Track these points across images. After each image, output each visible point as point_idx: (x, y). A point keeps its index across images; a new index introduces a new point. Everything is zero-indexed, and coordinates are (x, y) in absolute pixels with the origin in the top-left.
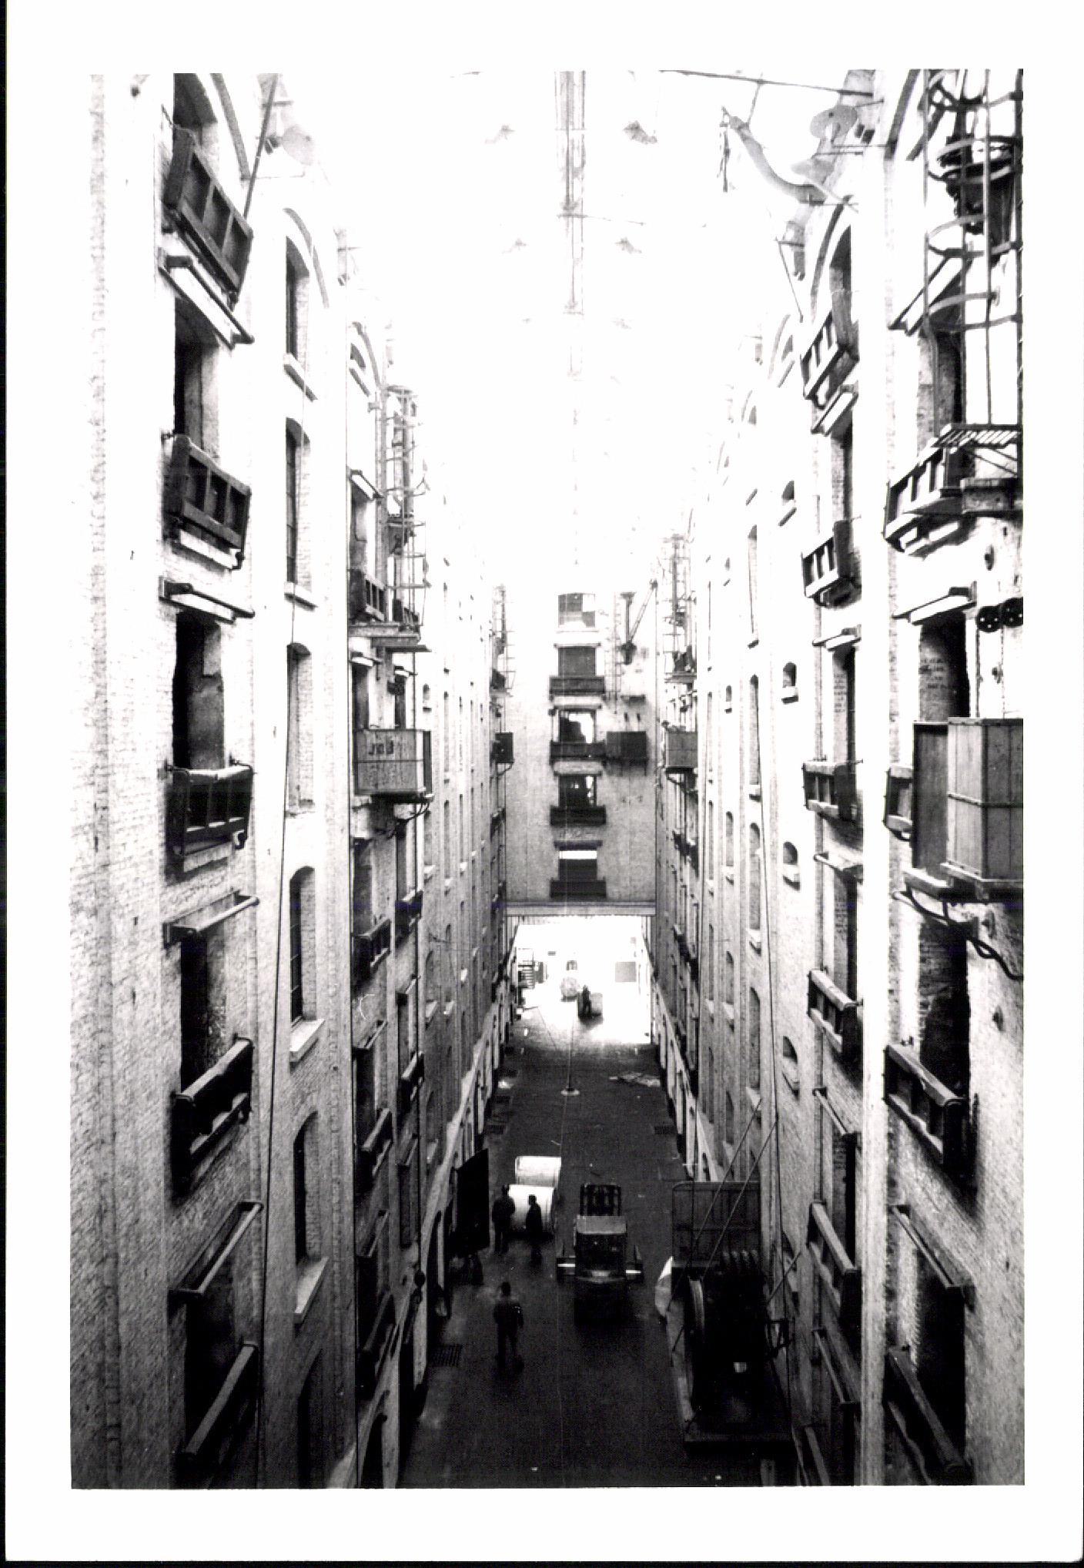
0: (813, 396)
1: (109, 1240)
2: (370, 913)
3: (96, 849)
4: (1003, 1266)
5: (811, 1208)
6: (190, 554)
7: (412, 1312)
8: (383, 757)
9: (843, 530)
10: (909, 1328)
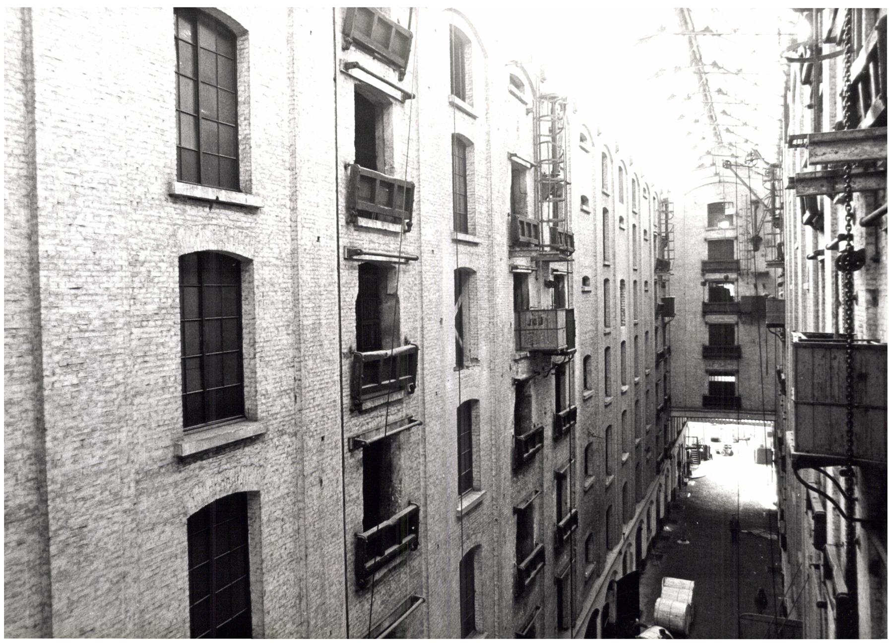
6: (368, 230)
8: (536, 327)
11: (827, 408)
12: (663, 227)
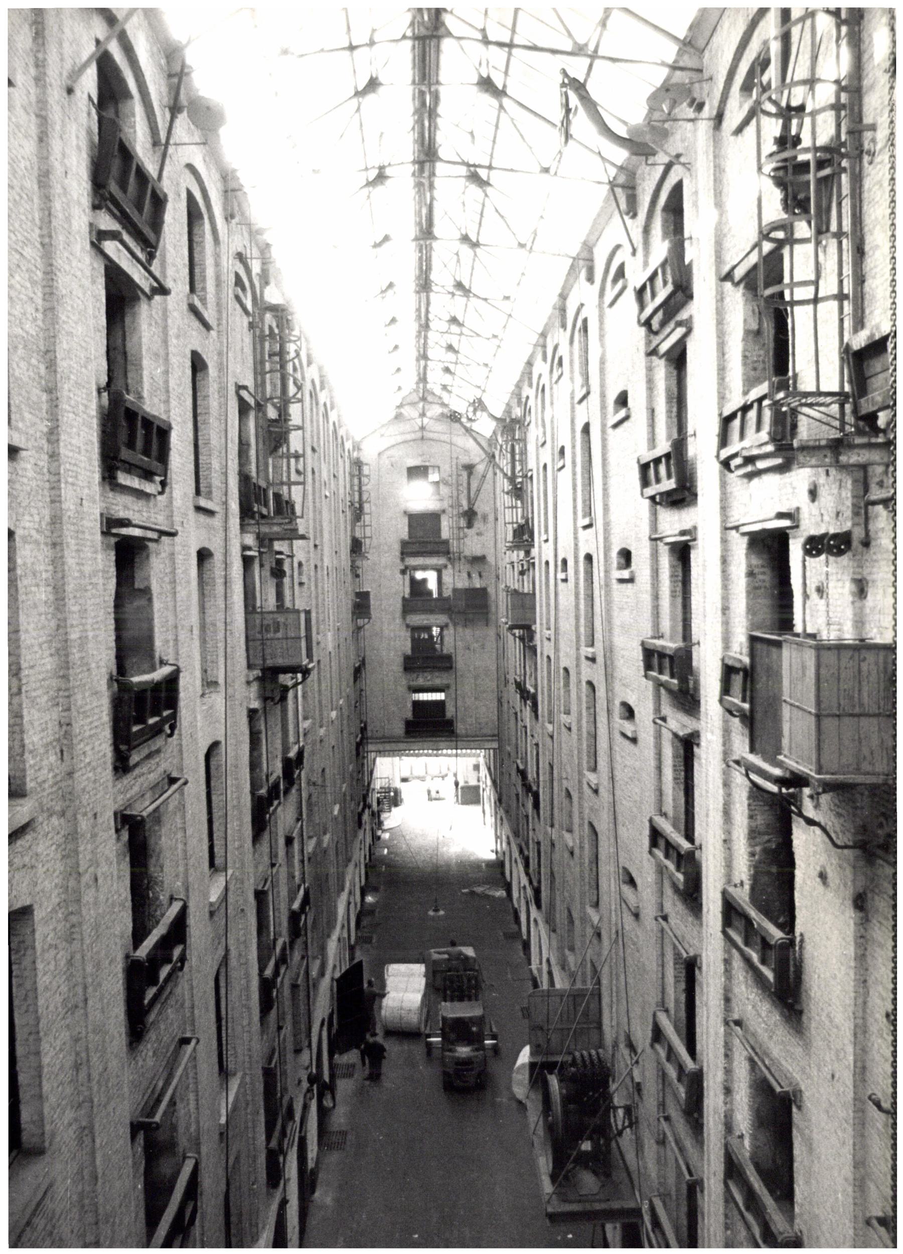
0: (647, 324)
1: (84, 1089)
2: (261, 770)
3: (62, 759)
4: (829, 1076)
5: (654, 1015)
7: (306, 1107)
8: (270, 635)
9: (680, 444)
10: (743, 1121)
11: (856, 719)
12: (357, 494)
